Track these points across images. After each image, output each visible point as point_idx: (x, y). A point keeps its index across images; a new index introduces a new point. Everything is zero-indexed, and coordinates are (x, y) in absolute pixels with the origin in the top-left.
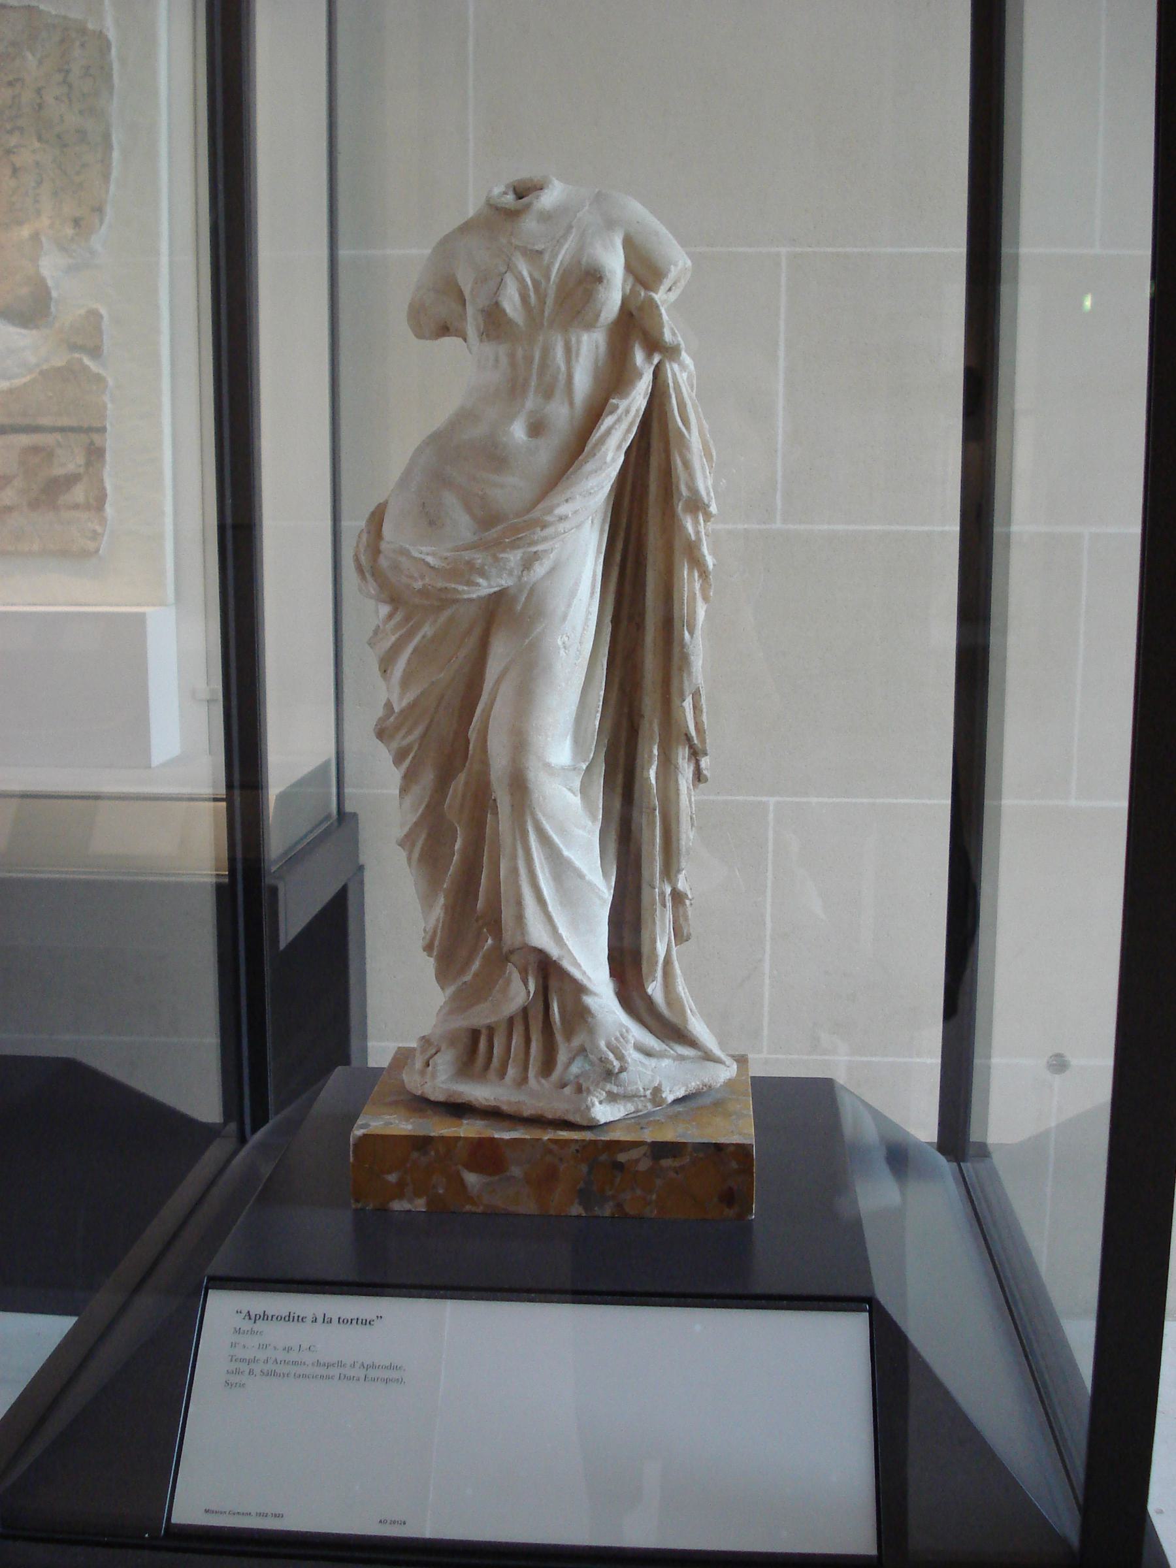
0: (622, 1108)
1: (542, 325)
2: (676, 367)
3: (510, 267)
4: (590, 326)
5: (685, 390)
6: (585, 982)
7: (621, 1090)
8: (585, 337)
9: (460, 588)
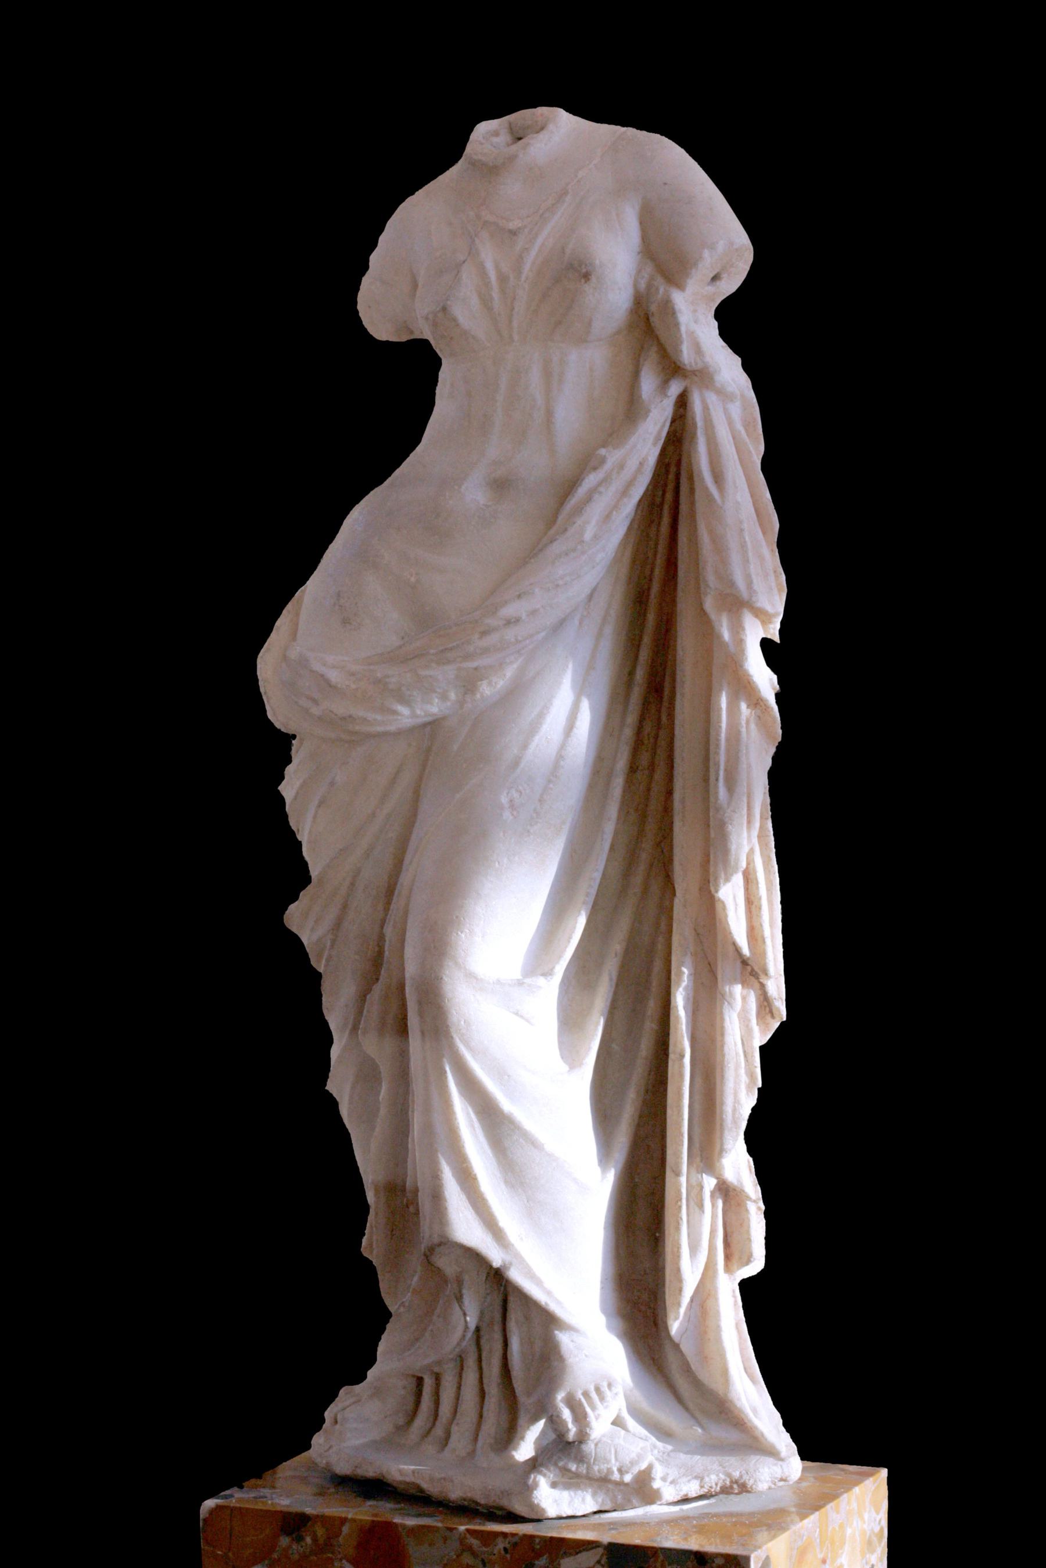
0: (589, 1498)
1: (511, 337)
2: (712, 398)
3: (472, 252)
4: (582, 340)
5: (723, 433)
6: (553, 1307)
7: (583, 1469)
8: (573, 356)
9: (370, 716)
